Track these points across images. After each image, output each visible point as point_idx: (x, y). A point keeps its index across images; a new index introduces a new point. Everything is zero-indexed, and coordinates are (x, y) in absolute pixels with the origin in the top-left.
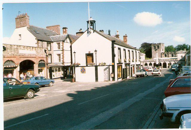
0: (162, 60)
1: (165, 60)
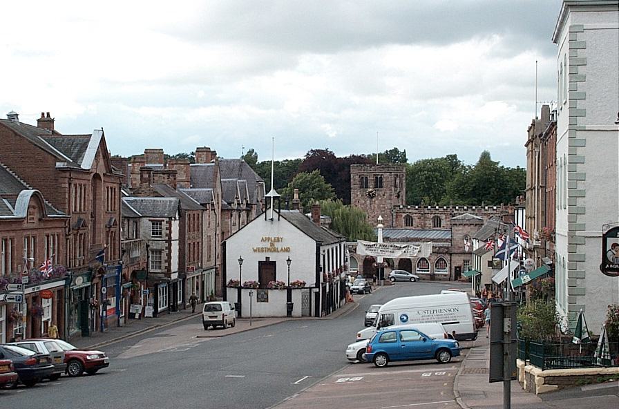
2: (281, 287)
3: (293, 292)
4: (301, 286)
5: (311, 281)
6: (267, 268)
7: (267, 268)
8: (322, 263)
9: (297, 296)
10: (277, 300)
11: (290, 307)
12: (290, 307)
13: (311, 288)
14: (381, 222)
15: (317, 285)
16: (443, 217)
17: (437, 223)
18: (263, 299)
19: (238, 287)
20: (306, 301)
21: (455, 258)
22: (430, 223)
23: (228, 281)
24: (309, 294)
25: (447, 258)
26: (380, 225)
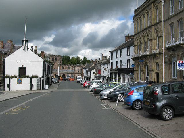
0: (62, 73)
1: (64, 73)
2: (28, 77)
3: (33, 79)
4: (36, 77)
5: (40, 75)
6: (22, 71)
7: (22, 71)
8: (45, 68)
9: (34, 81)
10: (26, 82)
11: (32, 86)
12: (32, 86)
13: (40, 78)
14: (59, 65)
15: (43, 77)
16: (70, 67)
17: (69, 68)
18: (19, 82)
19: (10, 78)
20: (38, 82)
21: (76, 75)
22: (67, 68)
23: (5, 76)
24: (39, 80)
25: (74, 74)
26: (59, 66)
